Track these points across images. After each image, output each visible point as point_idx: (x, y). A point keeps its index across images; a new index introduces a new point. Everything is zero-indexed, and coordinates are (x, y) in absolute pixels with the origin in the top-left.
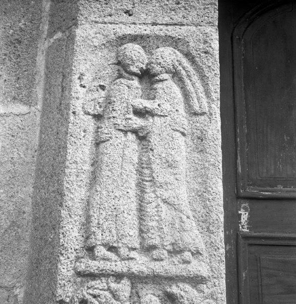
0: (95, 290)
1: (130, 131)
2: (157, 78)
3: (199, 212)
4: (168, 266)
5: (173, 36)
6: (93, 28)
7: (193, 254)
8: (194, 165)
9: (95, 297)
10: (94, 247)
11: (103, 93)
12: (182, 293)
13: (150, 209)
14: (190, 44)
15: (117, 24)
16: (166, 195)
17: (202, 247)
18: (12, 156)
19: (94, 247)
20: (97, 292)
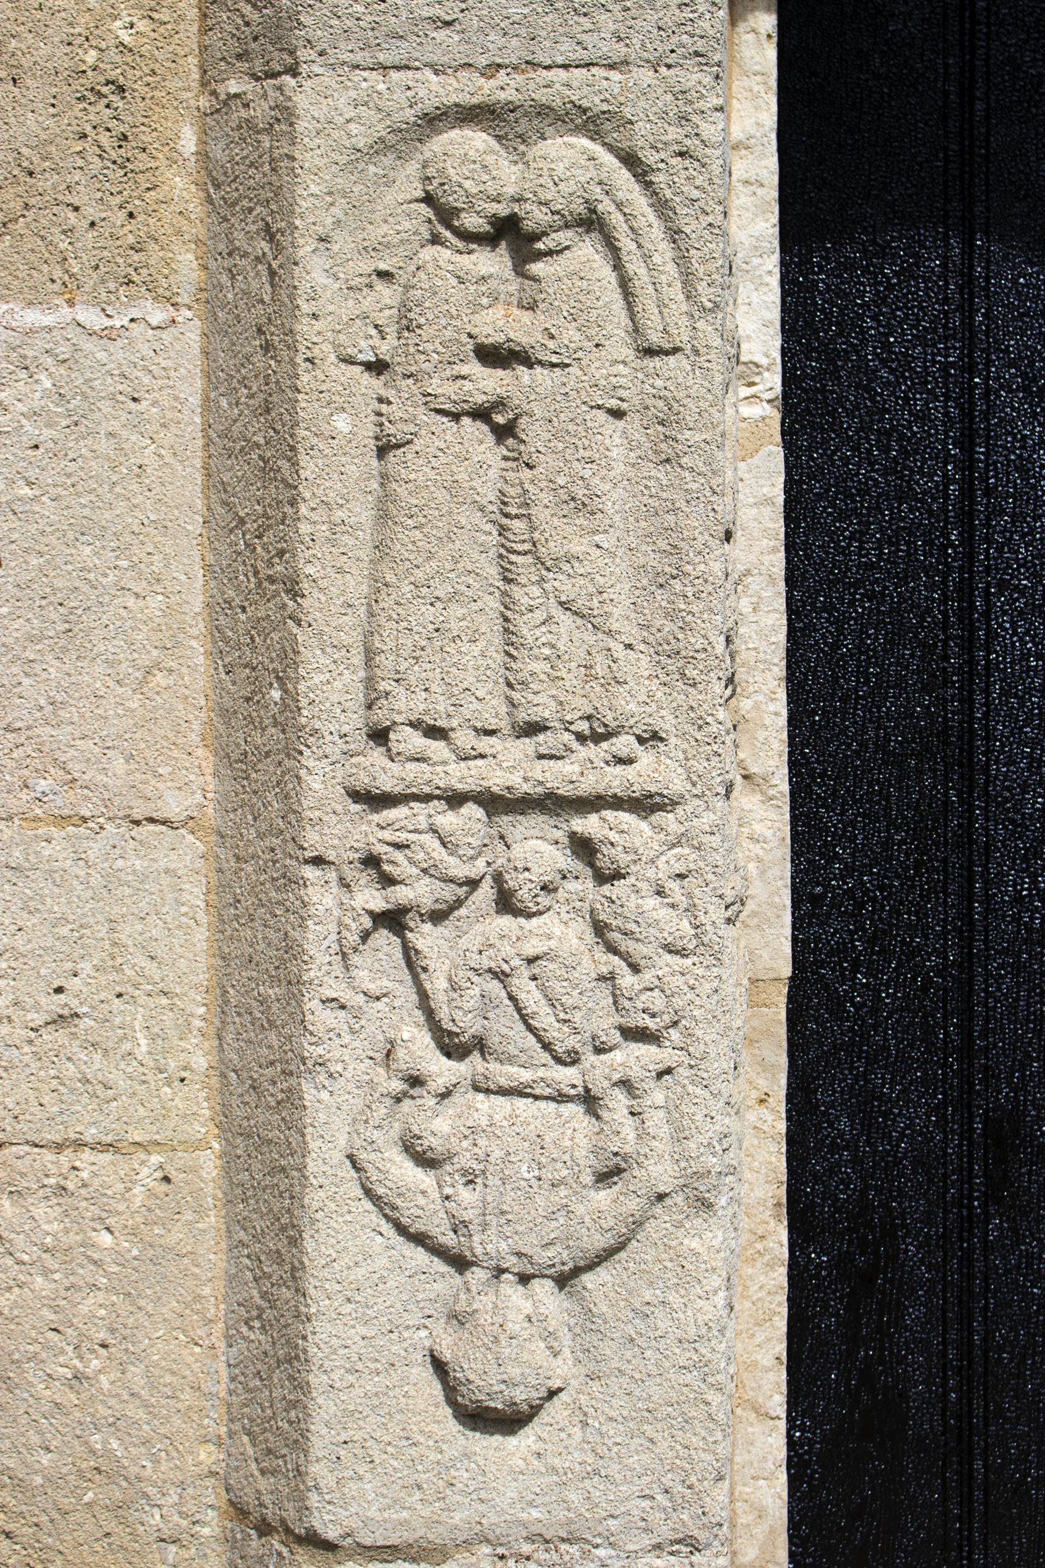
0: (398, 833)
1: (468, 414)
2: (542, 247)
3: (659, 630)
4: (579, 771)
5: (585, 103)
6: (347, 88)
7: (641, 740)
8: (645, 500)
9: (398, 846)
10: (387, 730)
11: (386, 293)
12: (613, 836)
13: (525, 626)
14: (636, 127)
15: (417, 69)
16: (567, 588)
17: (666, 723)
18: (139, 462)
19: (387, 730)
20: (403, 837)
